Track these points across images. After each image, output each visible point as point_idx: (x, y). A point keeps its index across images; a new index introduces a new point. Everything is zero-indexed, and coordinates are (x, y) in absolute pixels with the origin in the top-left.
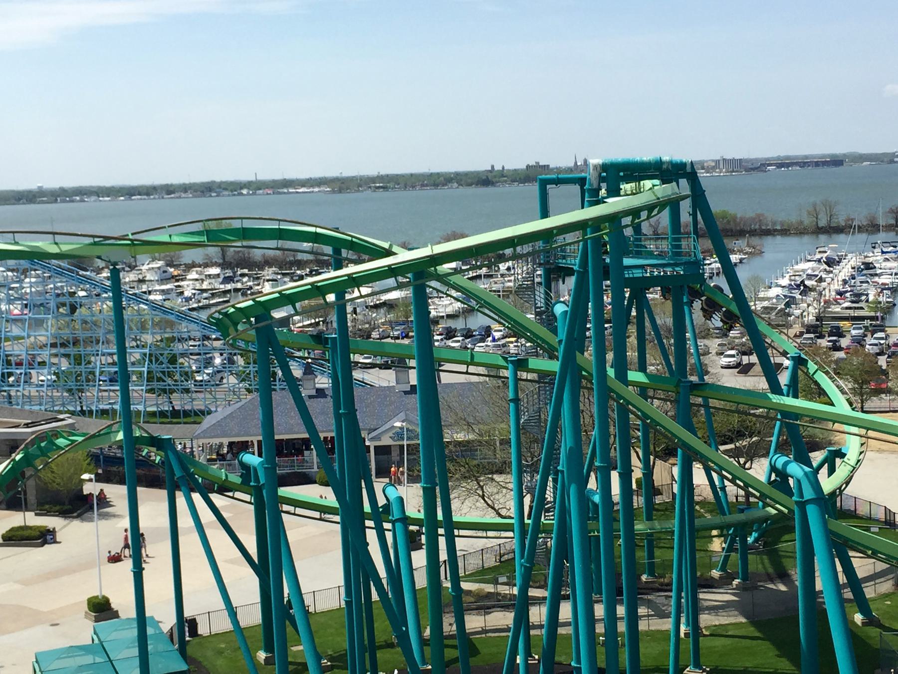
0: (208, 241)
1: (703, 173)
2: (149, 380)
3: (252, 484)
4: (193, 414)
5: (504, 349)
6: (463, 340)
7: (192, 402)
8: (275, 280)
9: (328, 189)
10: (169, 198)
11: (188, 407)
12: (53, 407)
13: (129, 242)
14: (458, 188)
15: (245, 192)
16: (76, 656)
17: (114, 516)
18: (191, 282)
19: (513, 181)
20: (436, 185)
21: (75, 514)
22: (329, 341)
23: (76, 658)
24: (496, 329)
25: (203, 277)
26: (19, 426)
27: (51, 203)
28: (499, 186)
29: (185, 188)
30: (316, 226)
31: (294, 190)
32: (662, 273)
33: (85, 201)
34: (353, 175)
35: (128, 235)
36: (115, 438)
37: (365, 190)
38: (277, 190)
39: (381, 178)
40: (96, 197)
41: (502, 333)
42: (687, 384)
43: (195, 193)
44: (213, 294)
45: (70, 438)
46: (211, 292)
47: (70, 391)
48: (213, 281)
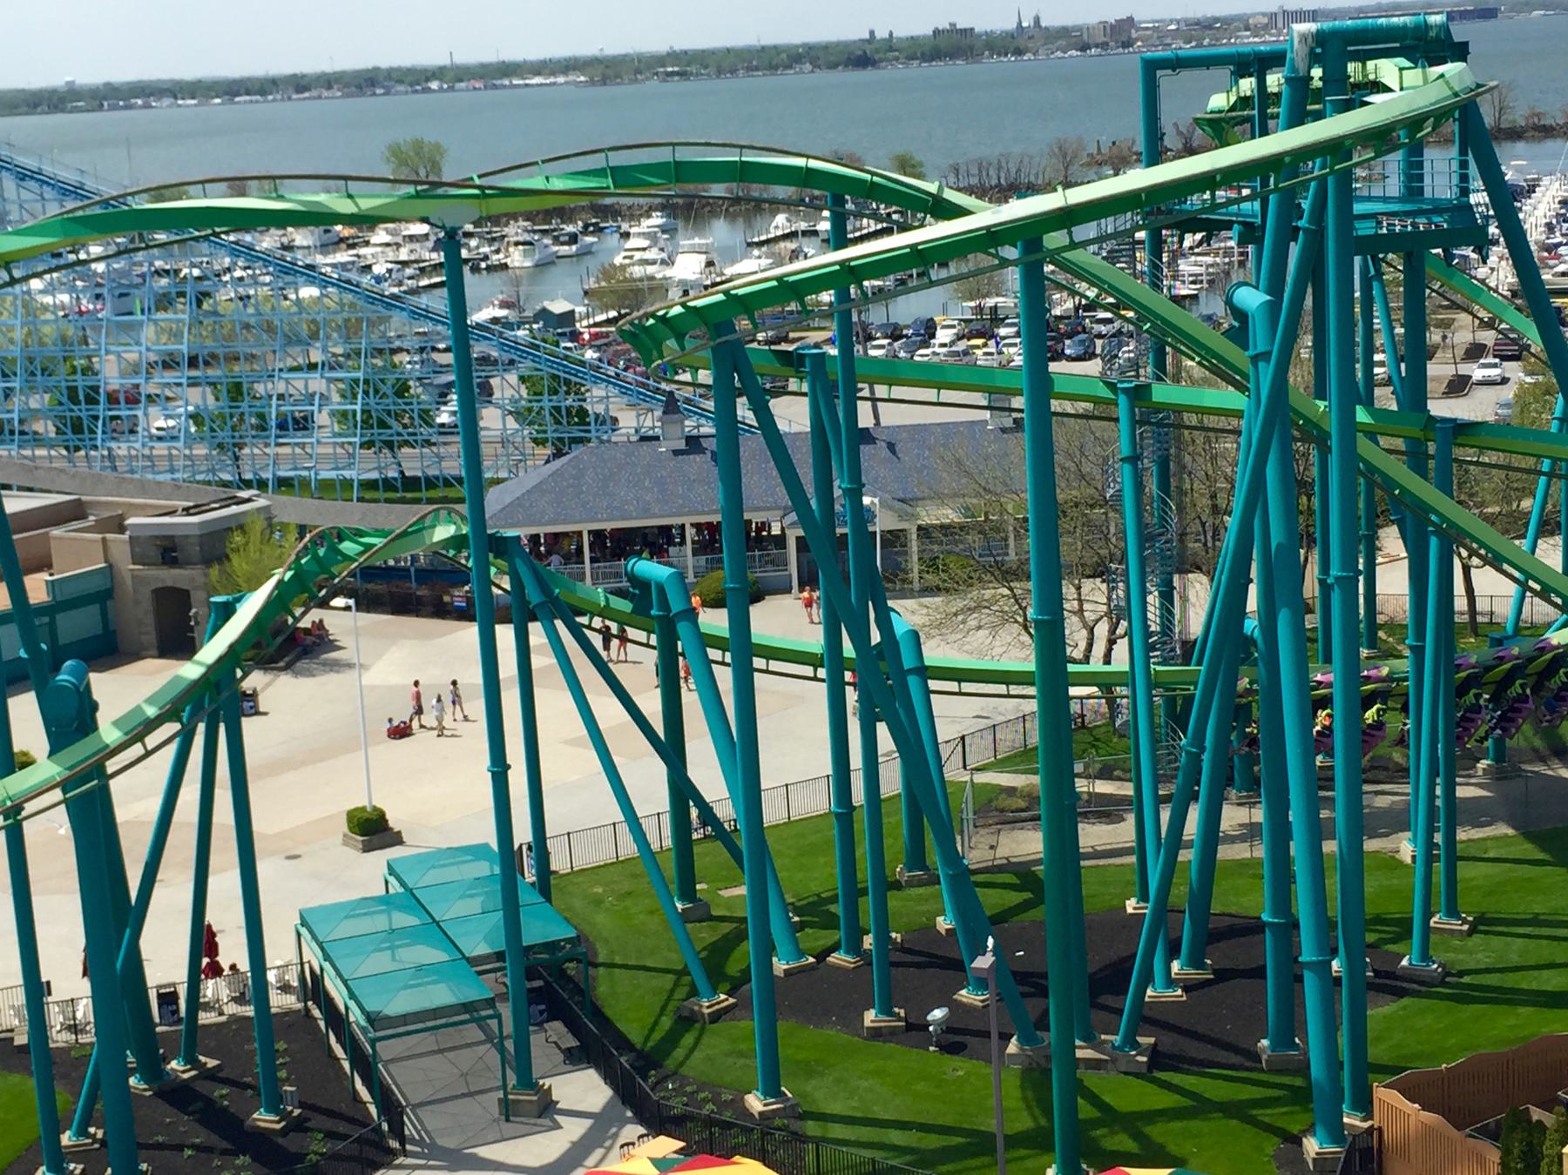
0: (615, 187)
1: (1248, 37)
2: (366, 424)
3: (654, 612)
4: (441, 484)
5: (966, 359)
6: (889, 344)
7: (440, 463)
8: (530, 243)
9: (582, 78)
10: (299, 99)
11: (433, 472)
12: (194, 476)
13: (476, 192)
14: (812, 72)
15: (434, 85)
16: (375, 912)
17: (350, 666)
18: (379, 249)
19: (912, 58)
20: (772, 68)
21: (281, 664)
22: (807, 361)
23: (375, 916)
24: (945, 323)
25: (399, 240)
26: (175, 512)
27: (93, 111)
28: (884, 68)
29: (328, 81)
30: (808, 157)
31: (521, 82)
32: (1409, 228)
33: (151, 107)
34: (623, 52)
35: (472, 179)
36: (431, 538)
37: (647, 79)
38: (490, 82)
39: (674, 56)
40: (172, 100)
41: (955, 331)
42: (1448, 425)
43: (346, 90)
44: (422, 270)
45: (362, 540)
46: (416, 266)
47: (220, 446)
48: (417, 246)
